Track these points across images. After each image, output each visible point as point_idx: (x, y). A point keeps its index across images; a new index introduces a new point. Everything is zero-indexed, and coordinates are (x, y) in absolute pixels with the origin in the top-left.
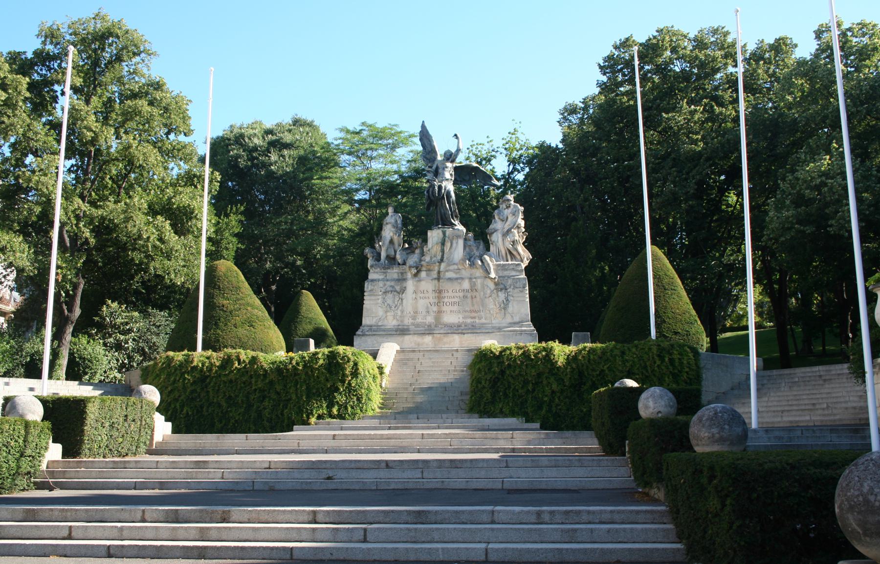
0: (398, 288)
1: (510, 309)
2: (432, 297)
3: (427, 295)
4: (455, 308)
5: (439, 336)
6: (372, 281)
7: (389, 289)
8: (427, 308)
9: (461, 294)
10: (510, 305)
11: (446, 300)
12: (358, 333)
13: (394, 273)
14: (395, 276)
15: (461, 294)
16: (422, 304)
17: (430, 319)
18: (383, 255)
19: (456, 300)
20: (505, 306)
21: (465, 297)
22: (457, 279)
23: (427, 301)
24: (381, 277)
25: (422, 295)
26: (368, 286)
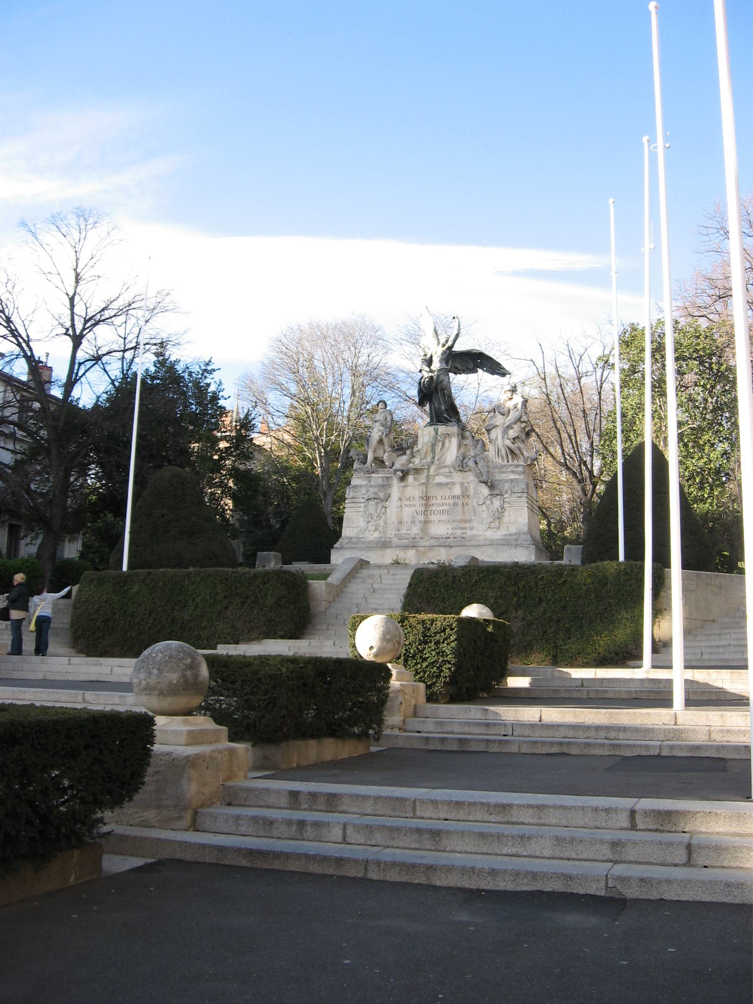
0: (381, 495)
1: (506, 519)
2: (419, 505)
3: (413, 503)
4: (444, 517)
5: (423, 549)
6: (354, 487)
7: (372, 496)
8: (413, 517)
9: (451, 501)
10: (506, 514)
11: (434, 508)
12: (335, 546)
13: (378, 478)
14: (380, 481)
15: (451, 501)
16: (407, 512)
17: (415, 530)
18: (370, 457)
19: (445, 508)
20: (498, 516)
21: (455, 504)
22: (447, 484)
23: (413, 509)
24: (364, 483)
25: (407, 503)
26: (349, 493)
